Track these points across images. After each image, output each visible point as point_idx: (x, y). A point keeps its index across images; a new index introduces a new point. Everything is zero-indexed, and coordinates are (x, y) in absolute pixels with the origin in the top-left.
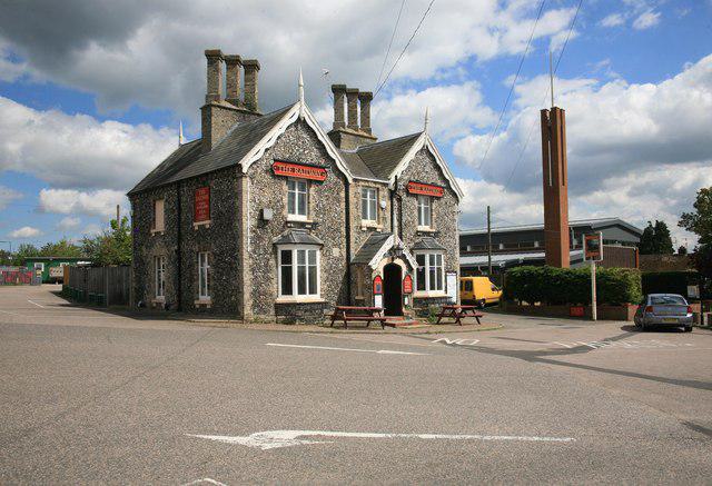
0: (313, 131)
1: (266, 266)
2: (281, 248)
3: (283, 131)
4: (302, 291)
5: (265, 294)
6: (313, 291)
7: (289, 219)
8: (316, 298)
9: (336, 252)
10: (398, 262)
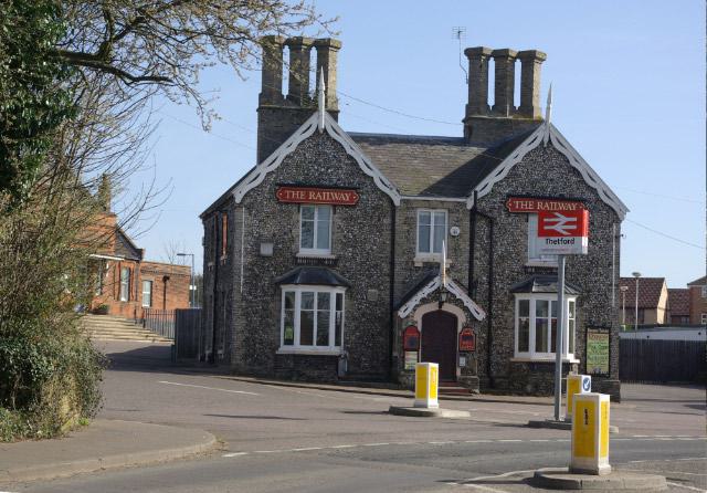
7: (527, 264)
8: (332, 349)
10: (449, 308)
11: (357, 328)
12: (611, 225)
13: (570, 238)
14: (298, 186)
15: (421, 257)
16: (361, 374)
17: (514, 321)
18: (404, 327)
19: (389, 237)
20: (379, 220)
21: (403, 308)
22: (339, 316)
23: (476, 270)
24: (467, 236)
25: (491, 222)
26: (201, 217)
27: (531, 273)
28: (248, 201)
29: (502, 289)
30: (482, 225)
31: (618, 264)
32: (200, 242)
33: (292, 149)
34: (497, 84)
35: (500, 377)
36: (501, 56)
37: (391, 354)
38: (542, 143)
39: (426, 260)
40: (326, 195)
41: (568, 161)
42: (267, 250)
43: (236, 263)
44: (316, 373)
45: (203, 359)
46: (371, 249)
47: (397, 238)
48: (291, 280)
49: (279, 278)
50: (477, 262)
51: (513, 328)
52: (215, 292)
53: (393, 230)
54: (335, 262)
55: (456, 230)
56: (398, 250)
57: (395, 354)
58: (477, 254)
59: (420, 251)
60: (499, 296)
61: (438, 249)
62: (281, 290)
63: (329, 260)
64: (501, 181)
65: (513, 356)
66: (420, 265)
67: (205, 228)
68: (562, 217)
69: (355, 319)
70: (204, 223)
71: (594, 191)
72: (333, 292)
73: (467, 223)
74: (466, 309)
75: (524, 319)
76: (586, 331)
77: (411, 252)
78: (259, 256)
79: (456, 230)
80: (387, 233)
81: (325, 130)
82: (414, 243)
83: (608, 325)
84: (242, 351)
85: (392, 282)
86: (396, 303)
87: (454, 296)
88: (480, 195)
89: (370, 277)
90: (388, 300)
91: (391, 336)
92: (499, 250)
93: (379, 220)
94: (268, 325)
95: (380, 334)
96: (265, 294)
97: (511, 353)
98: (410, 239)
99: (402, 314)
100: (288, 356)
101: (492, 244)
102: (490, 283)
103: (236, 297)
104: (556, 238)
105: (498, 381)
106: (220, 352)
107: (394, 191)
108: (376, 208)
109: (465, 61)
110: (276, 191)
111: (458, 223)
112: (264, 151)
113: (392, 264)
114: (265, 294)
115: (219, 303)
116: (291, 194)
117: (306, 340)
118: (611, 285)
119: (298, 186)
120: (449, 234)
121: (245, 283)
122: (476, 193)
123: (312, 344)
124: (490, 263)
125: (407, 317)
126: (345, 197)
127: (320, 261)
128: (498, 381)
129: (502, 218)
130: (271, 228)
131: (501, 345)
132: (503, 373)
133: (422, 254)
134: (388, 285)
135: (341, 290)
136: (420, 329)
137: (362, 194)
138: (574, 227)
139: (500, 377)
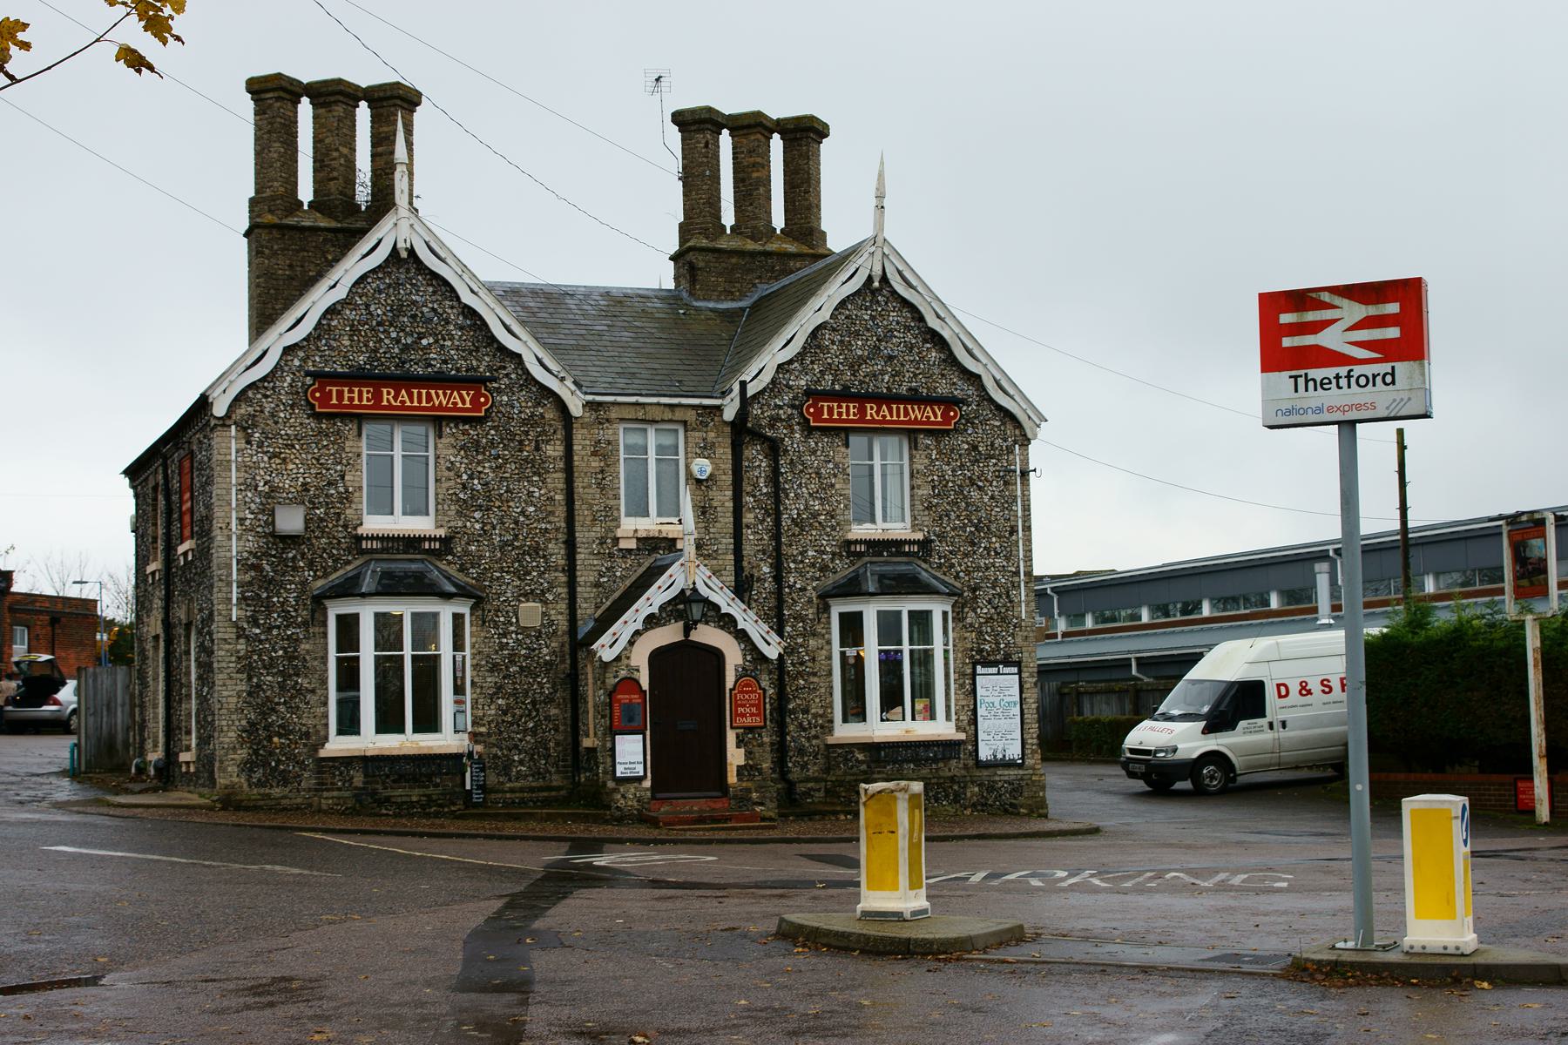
0: (446, 283)
1: (290, 657)
2: (335, 609)
3: (825, 315)
4: (389, 721)
5: (285, 731)
6: (428, 721)
7: (851, 536)
8: (447, 740)
9: (530, 613)
10: (708, 635)
11: (499, 688)
12: (1010, 451)
13: (1385, 367)
14: (356, 377)
15: (631, 526)
16: (512, 790)
17: (829, 658)
18: (611, 681)
19: (562, 486)
20: (537, 448)
21: (606, 639)
22: (459, 659)
23: (748, 550)
24: (728, 478)
25: (774, 449)
26: (127, 472)
27: (860, 555)
28: (243, 410)
29: (803, 589)
30: (755, 455)
31: (1028, 529)
32: (127, 527)
33: (341, 293)
34: (738, 181)
35: (808, 780)
36: (752, 128)
37: (576, 743)
38: (870, 279)
39: (641, 534)
40: (417, 399)
41: (921, 319)
42: (291, 520)
43: (217, 555)
44: (415, 795)
45: (141, 770)
46: (523, 513)
47: (579, 484)
48: (348, 589)
49: (320, 583)
50: (749, 535)
51: (830, 673)
52: (167, 625)
53: (569, 470)
54: (446, 542)
55: (702, 467)
56: (582, 513)
57: (587, 742)
58: (749, 518)
59: (628, 515)
60: (801, 606)
61: (670, 507)
62: (325, 609)
63: (430, 539)
64: (790, 362)
65: (831, 731)
66: (632, 545)
67: (137, 496)
68: (1345, 303)
69: (494, 668)
70: (133, 487)
71: (974, 379)
72: (446, 612)
73: (724, 452)
74: (742, 636)
75: (851, 652)
76: (974, 674)
77: (610, 516)
78: (273, 534)
79: (702, 467)
80: (556, 480)
81: (411, 252)
82: (617, 497)
83: (1015, 658)
84: (243, 754)
85: (572, 584)
86: (584, 629)
87: (716, 607)
88: (751, 390)
89: (522, 574)
90: (562, 622)
91: (575, 699)
92: (792, 508)
93: (537, 448)
94: (300, 691)
95: (549, 700)
96: (289, 621)
97: (828, 727)
98: (604, 483)
99: (606, 649)
100: (348, 761)
101: (777, 493)
102: (778, 578)
103: (221, 631)
104: (1330, 372)
105: (801, 788)
106: (184, 757)
107: (569, 383)
108: (532, 421)
109: (674, 136)
110: (306, 388)
111: (706, 450)
112: (263, 317)
113: (571, 545)
114: (289, 621)
115: (179, 648)
116: (340, 395)
117: (389, 721)
118: (1017, 573)
119: (356, 377)
120: (689, 474)
121: (243, 599)
122: (743, 385)
123: (401, 730)
124: (776, 536)
125: (618, 659)
126: (461, 400)
127: (411, 543)
128: (801, 788)
129: (794, 441)
130: (296, 472)
131: (806, 711)
132: (813, 770)
133: (632, 520)
134: (563, 591)
135: (464, 608)
136: (645, 684)
137: (499, 390)
138: (1393, 333)
139: (808, 780)
